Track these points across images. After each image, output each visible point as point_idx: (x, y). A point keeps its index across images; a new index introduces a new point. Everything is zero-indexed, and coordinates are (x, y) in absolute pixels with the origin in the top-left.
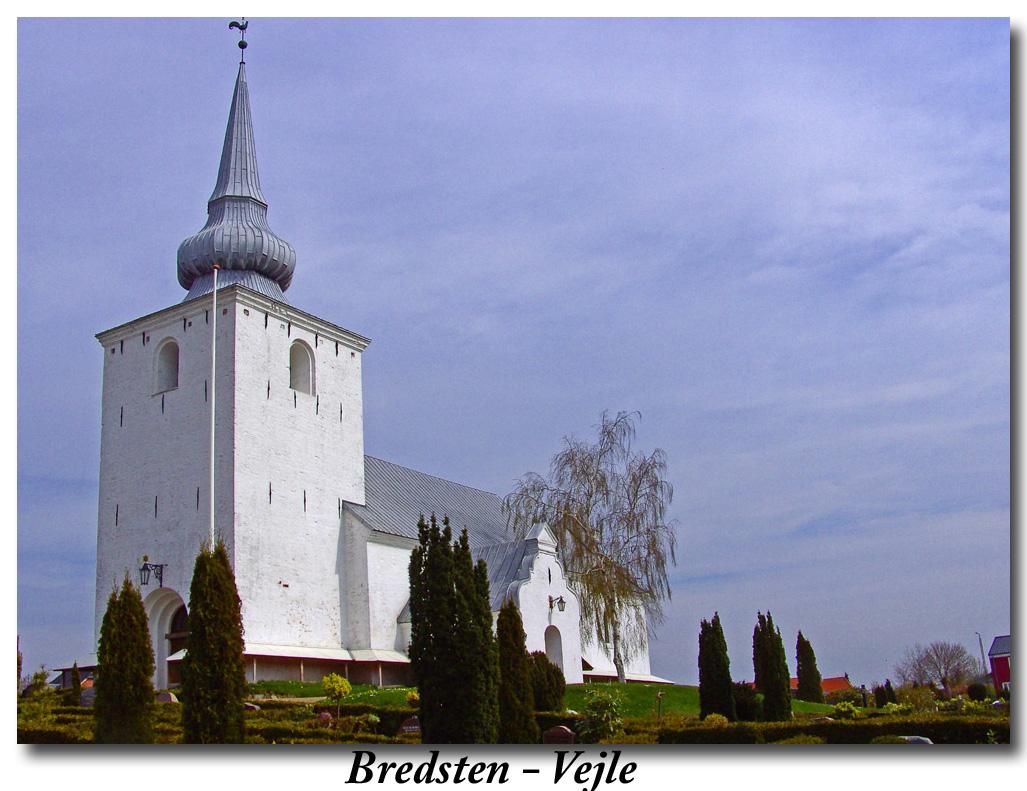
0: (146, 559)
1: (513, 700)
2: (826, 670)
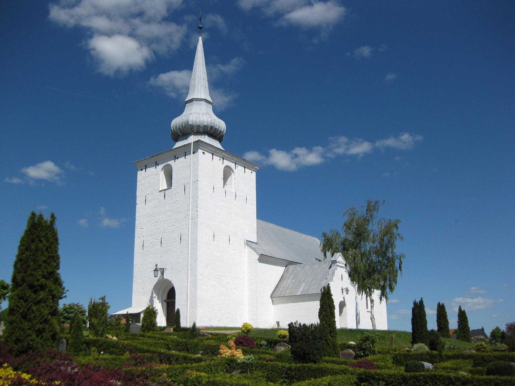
0: (156, 266)
1: (369, 373)
2: (473, 325)
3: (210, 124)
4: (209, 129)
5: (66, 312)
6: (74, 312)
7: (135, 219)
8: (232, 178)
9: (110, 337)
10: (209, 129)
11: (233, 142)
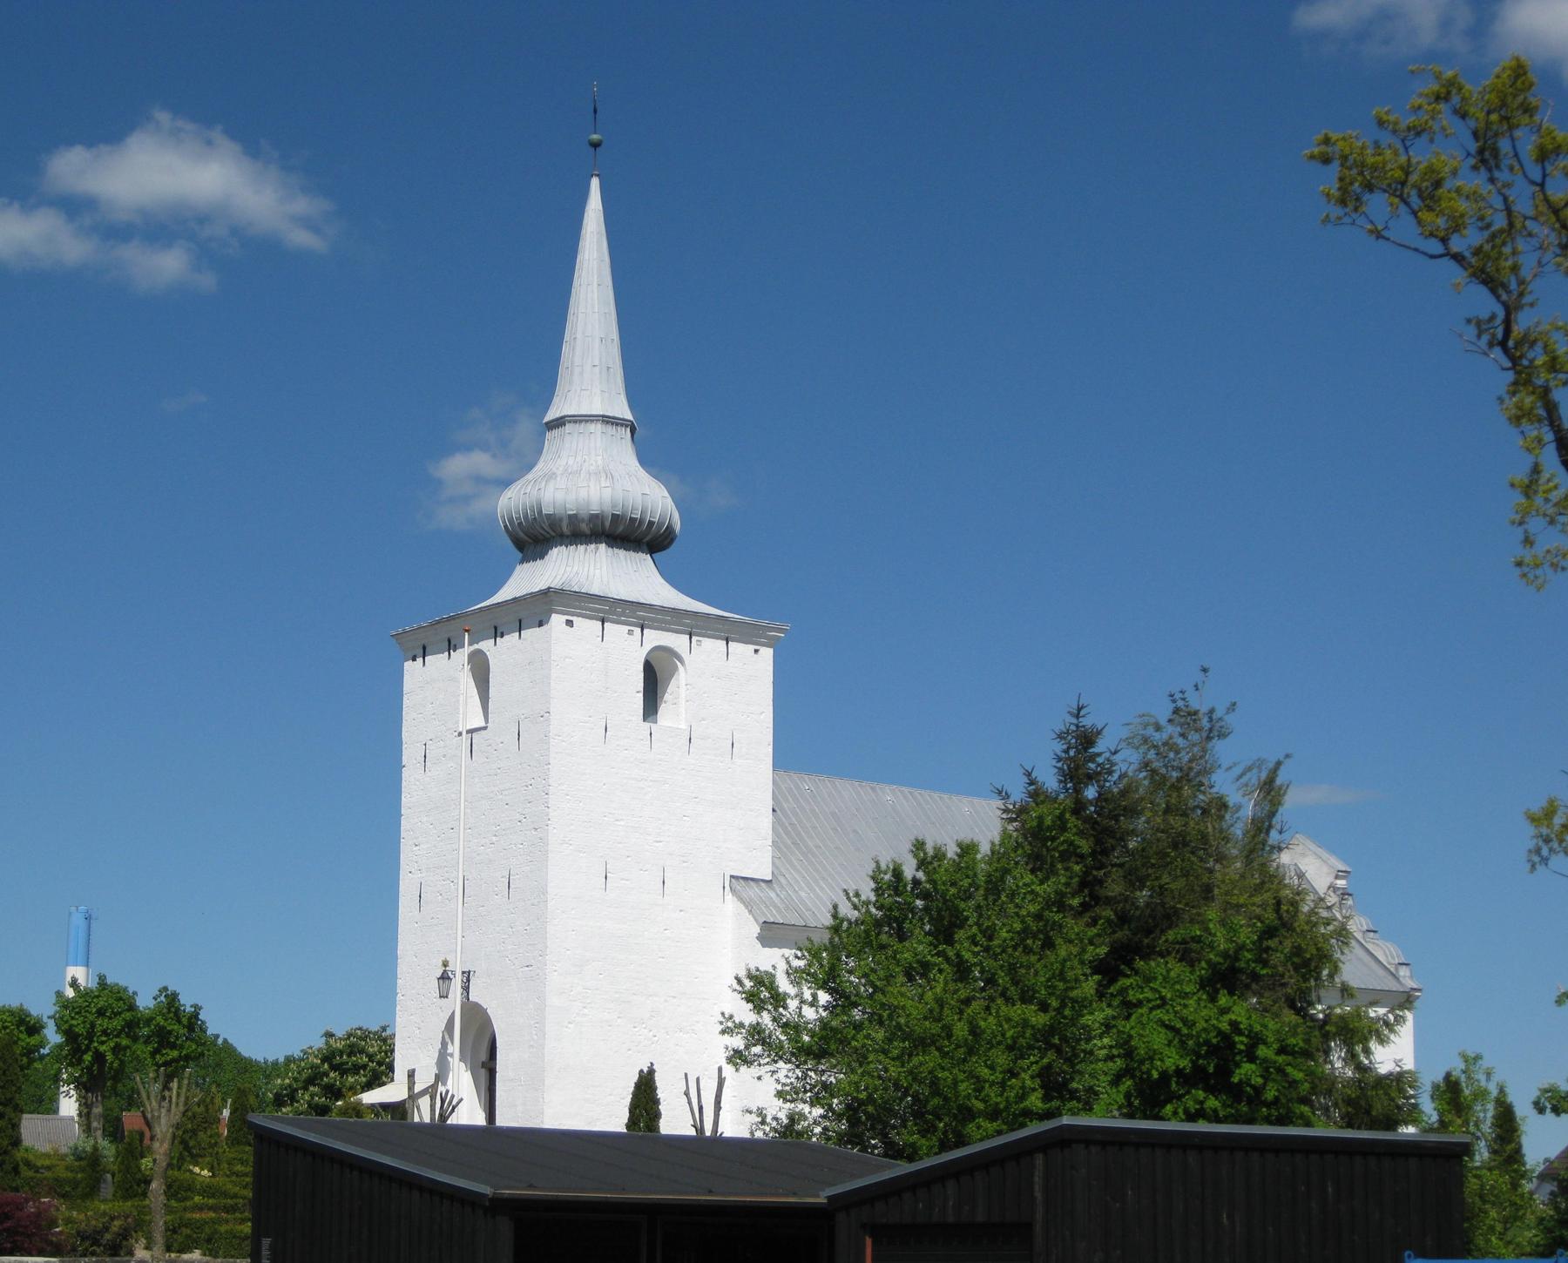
3: (609, 510)
4: (607, 524)
5: (334, 1068)
6: (364, 1067)
7: (397, 815)
8: (677, 691)
9: (197, 1170)
10: (607, 524)
11: (708, 556)
